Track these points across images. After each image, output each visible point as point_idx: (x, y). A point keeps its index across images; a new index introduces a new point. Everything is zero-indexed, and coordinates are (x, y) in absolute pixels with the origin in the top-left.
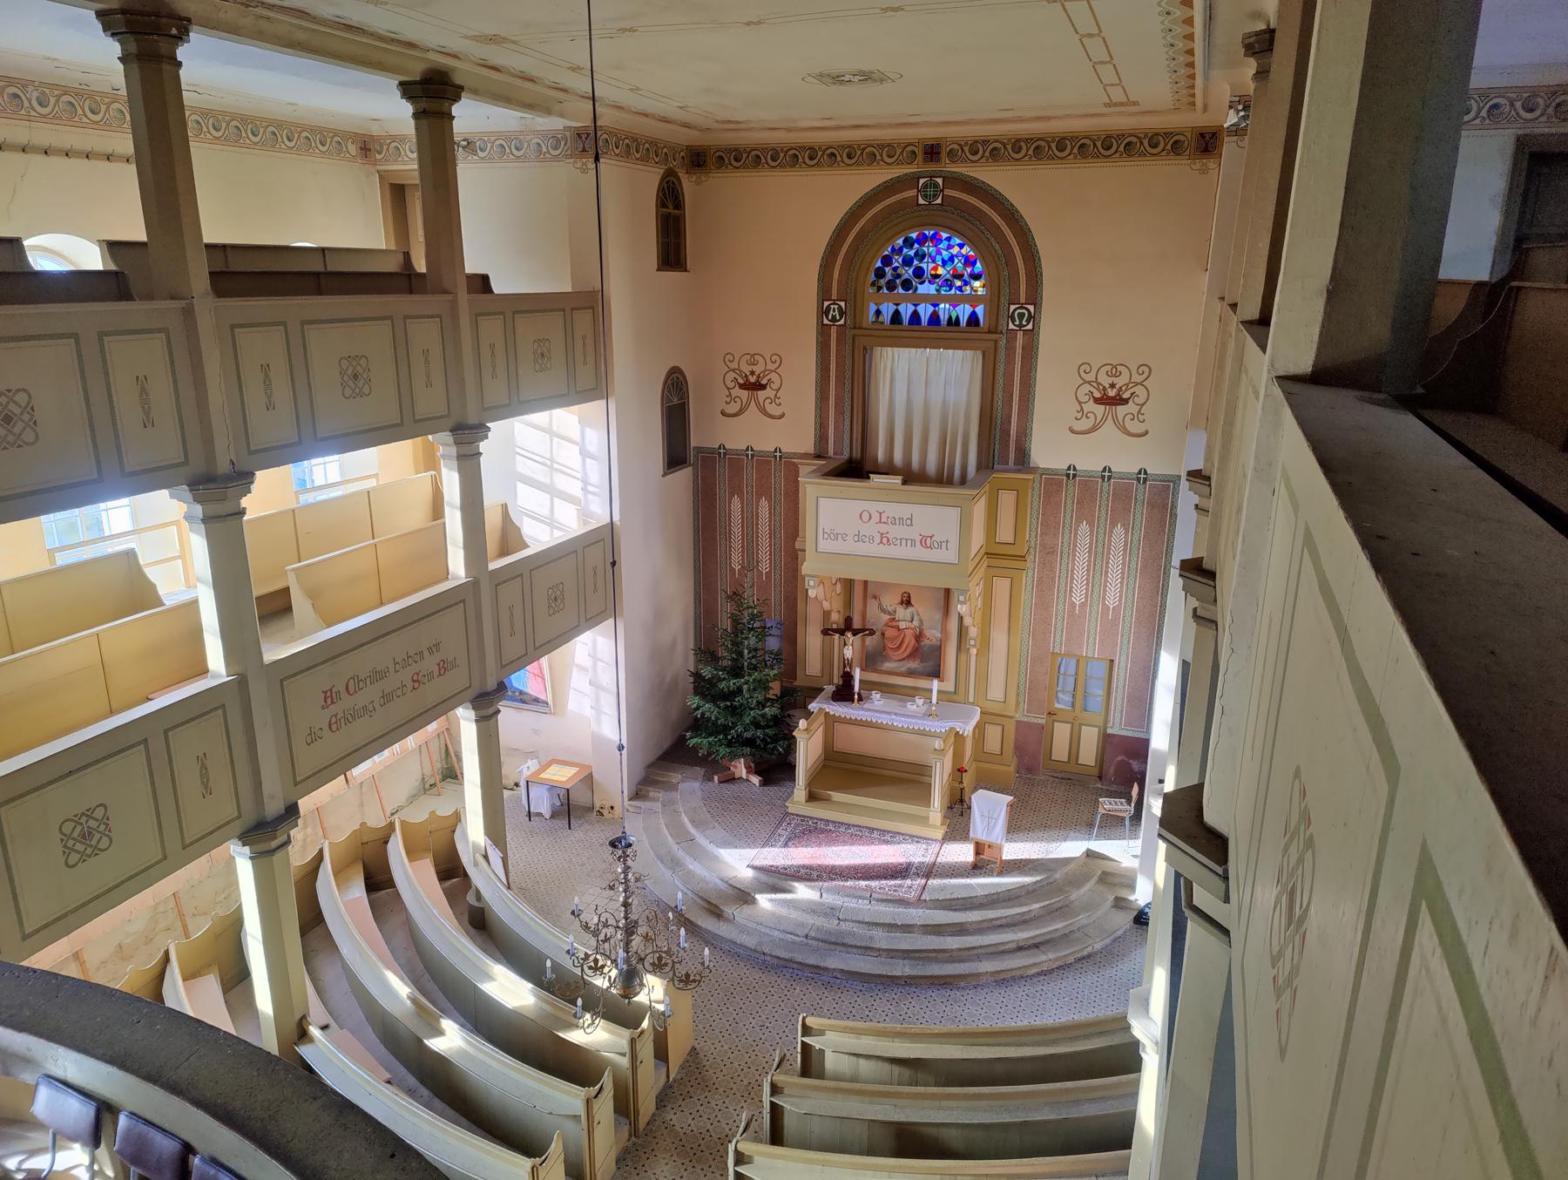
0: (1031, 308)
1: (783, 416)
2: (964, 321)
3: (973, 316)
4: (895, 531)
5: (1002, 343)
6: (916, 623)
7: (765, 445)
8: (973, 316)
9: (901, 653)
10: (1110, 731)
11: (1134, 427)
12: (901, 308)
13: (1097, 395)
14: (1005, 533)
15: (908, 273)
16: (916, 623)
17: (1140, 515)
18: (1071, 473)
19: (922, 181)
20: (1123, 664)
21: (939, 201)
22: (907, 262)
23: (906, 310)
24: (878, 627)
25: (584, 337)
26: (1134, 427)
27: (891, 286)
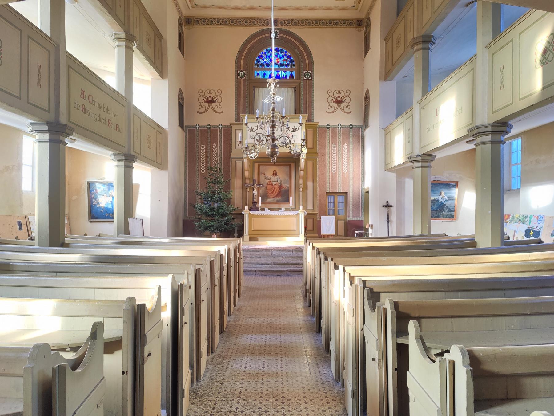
0: (311, 72)
1: (222, 112)
2: (288, 77)
3: (291, 75)
5: (302, 84)
6: (279, 182)
8: (291, 75)
9: (273, 195)
13: (334, 100)
16: (279, 182)
17: (352, 139)
18: (328, 127)
26: (347, 110)
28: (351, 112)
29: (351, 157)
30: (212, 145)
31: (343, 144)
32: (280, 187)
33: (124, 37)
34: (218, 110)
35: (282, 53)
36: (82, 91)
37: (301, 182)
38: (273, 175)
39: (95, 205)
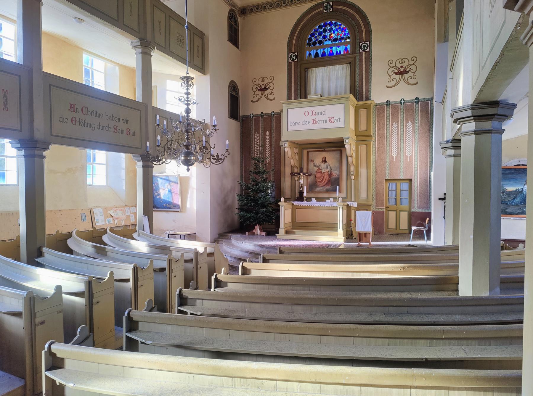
0: (368, 43)
1: (275, 99)
3: (346, 49)
4: (318, 118)
5: (357, 58)
6: (329, 169)
7: (268, 110)
9: (325, 182)
10: (413, 210)
11: (412, 81)
12: (318, 51)
13: (396, 71)
14: (363, 127)
15: (321, 38)
16: (329, 169)
17: (418, 117)
19: (324, 4)
20: (416, 180)
21: (331, 10)
22: (320, 34)
23: (320, 52)
24: (314, 173)
25: (198, 47)
26: (412, 81)
27: (314, 44)
28: (417, 83)
29: (416, 137)
30: (265, 134)
31: (407, 122)
32: (330, 175)
33: (139, 44)
34: (271, 97)
35: (335, 26)
36: (71, 105)
37: (352, 168)
38: (323, 162)
39: (156, 196)
